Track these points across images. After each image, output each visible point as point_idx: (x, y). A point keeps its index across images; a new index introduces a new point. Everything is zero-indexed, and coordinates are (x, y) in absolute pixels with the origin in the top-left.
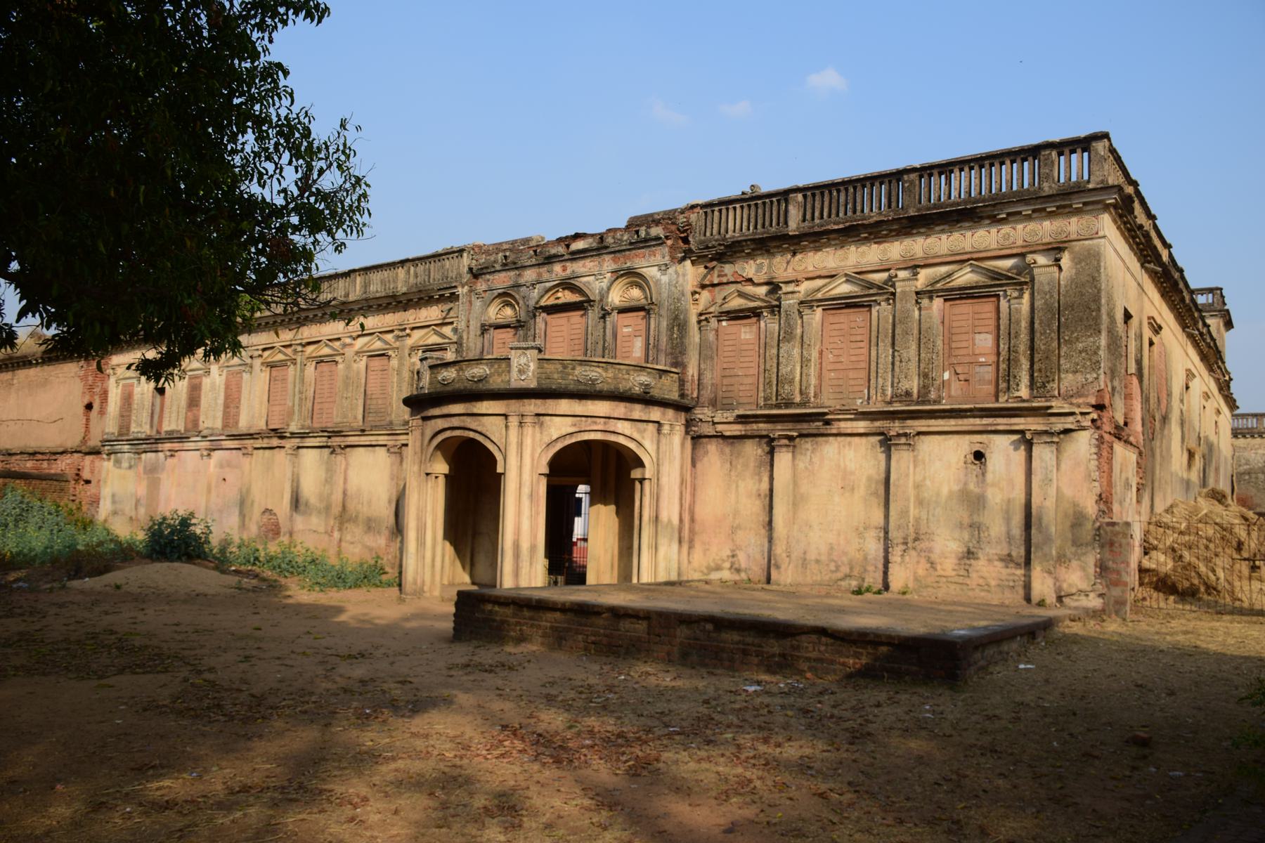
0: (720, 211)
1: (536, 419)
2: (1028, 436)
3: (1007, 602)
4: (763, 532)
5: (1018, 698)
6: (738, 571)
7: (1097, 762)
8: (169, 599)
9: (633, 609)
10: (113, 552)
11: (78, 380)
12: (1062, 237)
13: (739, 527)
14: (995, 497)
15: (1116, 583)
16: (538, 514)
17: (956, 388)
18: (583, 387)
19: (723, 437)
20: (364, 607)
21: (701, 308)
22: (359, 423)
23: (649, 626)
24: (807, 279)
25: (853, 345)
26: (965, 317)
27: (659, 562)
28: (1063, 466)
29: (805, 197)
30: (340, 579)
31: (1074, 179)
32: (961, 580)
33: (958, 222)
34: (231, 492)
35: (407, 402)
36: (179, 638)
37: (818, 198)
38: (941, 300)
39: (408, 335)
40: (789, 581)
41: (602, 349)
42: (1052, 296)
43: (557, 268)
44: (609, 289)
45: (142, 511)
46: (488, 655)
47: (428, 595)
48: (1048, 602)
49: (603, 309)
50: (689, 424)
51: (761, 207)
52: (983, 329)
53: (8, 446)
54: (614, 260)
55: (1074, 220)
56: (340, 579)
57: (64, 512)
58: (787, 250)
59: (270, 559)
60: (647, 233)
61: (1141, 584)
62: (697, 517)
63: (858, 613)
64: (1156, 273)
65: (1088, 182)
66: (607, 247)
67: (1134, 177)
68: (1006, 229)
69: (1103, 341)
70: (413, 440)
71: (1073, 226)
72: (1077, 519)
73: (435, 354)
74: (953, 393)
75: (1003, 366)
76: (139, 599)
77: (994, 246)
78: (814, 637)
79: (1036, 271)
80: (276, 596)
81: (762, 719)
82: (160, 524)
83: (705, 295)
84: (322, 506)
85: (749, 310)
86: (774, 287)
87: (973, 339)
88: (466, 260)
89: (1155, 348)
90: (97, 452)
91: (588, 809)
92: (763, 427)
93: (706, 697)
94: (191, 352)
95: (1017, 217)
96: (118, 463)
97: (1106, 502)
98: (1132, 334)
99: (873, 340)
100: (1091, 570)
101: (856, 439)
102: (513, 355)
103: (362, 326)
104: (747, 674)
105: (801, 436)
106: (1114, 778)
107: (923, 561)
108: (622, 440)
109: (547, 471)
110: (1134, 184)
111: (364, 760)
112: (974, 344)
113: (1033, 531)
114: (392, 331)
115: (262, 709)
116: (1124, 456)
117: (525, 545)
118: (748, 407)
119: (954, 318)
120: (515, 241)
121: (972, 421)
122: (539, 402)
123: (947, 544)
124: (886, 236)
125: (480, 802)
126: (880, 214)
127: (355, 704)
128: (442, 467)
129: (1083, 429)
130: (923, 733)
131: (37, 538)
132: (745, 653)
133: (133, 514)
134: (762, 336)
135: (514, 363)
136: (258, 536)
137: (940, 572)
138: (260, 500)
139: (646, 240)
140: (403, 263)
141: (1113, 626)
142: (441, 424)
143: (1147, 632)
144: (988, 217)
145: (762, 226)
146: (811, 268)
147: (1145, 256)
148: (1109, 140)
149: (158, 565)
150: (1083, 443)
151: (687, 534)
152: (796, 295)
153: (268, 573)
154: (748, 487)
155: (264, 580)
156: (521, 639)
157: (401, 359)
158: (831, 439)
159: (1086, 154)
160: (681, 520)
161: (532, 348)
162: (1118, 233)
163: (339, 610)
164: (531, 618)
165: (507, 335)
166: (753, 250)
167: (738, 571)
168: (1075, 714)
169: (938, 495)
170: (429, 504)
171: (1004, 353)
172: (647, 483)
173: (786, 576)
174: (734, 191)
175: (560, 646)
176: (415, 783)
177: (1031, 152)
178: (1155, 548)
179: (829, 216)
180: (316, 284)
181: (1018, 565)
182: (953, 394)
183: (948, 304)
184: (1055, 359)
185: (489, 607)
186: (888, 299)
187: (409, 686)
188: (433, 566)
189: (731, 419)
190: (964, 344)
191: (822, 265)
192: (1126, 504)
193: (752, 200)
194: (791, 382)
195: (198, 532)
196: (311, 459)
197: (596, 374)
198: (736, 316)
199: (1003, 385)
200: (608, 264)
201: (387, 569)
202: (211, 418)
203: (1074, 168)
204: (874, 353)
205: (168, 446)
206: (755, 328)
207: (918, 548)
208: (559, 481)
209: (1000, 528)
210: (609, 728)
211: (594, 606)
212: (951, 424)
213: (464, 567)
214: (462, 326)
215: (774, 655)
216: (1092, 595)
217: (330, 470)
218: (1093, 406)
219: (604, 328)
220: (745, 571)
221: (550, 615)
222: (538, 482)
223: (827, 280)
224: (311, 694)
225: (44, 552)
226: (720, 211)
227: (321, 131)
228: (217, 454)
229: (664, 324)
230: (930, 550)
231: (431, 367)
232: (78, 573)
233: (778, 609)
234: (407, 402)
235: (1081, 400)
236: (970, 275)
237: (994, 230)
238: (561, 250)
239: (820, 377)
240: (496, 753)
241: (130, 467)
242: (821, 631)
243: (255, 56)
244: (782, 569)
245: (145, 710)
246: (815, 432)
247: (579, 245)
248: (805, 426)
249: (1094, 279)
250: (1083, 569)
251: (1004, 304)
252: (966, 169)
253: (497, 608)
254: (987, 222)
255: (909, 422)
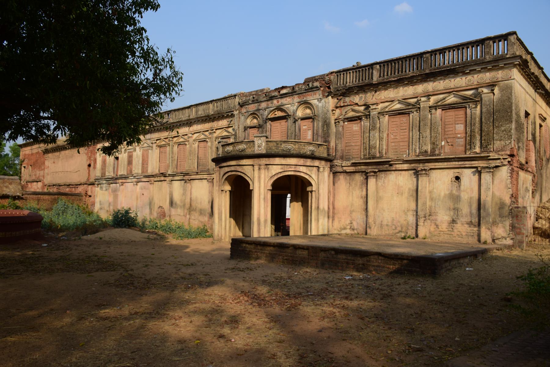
0: (344, 74)
1: (266, 167)
2: (479, 169)
3: (470, 242)
4: (364, 213)
5: (461, 282)
6: (353, 230)
7: (485, 308)
8: (120, 243)
9: (302, 245)
10: (100, 224)
11: (85, 155)
12: (495, 80)
13: (353, 211)
14: (465, 196)
15: (519, 234)
16: (267, 206)
17: (447, 149)
18: (285, 152)
19: (346, 172)
20: (197, 245)
21: (336, 117)
22: (196, 170)
23: (309, 253)
24: (382, 103)
25: (402, 131)
26: (451, 117)
27: (319, 226)
28: (495, 182)
29: (380, 66)
30: (189, 235)
31: (500, 53)
32: (449, 233)
33: (448, 75)
34: (146, 200)
35: (213, 160)
36: (122, 258)
37: (386, 67)
38: (441, 110)
39: (215, 132)
40: (375, 234)
41: (296, 136)
42: (490, 107)
43: (275, 101)
44: (297, 110)
45: (111, 208)
46: (243, 265)
47: (223, 241)
48: (488, 242)
49: (294, 119)
50: (331, 167)
51: (361, 71)
52: (459, 122)
53: (59, 182)
54: (299, 97)
55: (500, 72)
56: (189, 235)
57: (81, 209)
58: (373, 90)
59: (162, 227)
60: (313, 85)
61: (534, 234)
62: (336, 206)
63: (398, 246)
64: (543, 94)
65: (507, 54)
66: (295, 92)
67: (530, 50)
68: (469, 77)
69: (513, 126)
70: (215, 176)
71: (500, 74)
72: (501, 206)
73: (224, 140)
74: (446, 151)
75: (468, 138)
76: (109, 243)
77: (464, 85)
78: (376, 257)
79: (483, 96)
80: (163, 241)
81: (348, 289)
82: (118, 213)
83: (338, 111)
84: (182, 204)
85: (357, 117)
86: (367, 106)
87: (455, 127)
88: (237, 100)
89: (543, 128)
90: (93, 184)
91: (266, 322)
92: (363, 168)
93: (328, 281)
94: (120, 143)
95: (474, 72)
96: (101, 188)
97: (515, 198)
98: (530, 122)
99: (411, 129)
100: (508, 228)
101: (404, 172)
102: (255, 139)
103: (178, 132)
104: (347, 272)
105: (379, 171)
106: (488, 314)
107: (433, 224)
108: (302, 175)
109: (271, 188)
110: (531, 54)
111: (183, 303)
112: (455, 129)
113: (482, 211)
114: (208, 131)
115: (149, 285)
116: (525, 179)
117: (262, 220)
118: (357, 159)
119: (446, 118)
120: (258, 91)
121: (454, 163)
122: (267, 159)
123: (443, 217)
124: (416, 82)
125: (224, 319)
126: (413, 73)
127: (185, 283)
128: (228, 188)
129: (504, 165)
130: (414, 295)
131: (70, 219)
132: (348, 263)
133: (108, 209)
134: (362, 128)
135: (256, 143)
136: (157, 217)
137: (441, 230)
138: (157, 202)
139: (312, 88)
140: (211, 101)
141: (516, 252)
142: (227, 169)
143: (531, 255)
144: (461, 72)
145: (362, 80)
146: (383, 98)
147: (537, 87)
148: (517, 35)
149: (117, 230)
150: (504, 172)
151: (331, 214)
152: (377, 110)
153: (160, 232)
154: (357, 194)
155: (159, 235)
156: (257, 258)
157: (212, 142)
158: (393, 172)
159: (506, 42)
160: (329, 208)
161: (263, 136)
162: (522, 77)
163: (187, 247)
164: (261, 250)
165: (255, 131)
166: (358, 91)
167: (353, 230)
168: (483, 288)
169: (439, 196)
170: (223, 203)
171: (469, 133)
172: (313, 193)
173: (374, 232)
174: (350, 66)
175: (273, 261)
176: (202, 312)
177: (481, 42)
178: (541, 218)
179: (391, 74)
180: (161, 115)
181: (475, 226)
182: (446, 151)
183: (444, 111)
184: (491, 134)
185: (244, 245)
186: (417, 110)
187: (208, 276)
188: (225, 229)
189: (349, 165)
190: (451, 129)
191: (388, 96)
192: (526, 199)
193: (357, 69)
194: (375, 148)
195: (132, 216)
196: (177, 185)
197: (291, 147)
198: (351, 120)
199: (468, 147)
200: (296, 99)
201: (209, 230)
202: (137, 169)
203: (501, 48)
204: (411, 134)
205: (120, 181)
206: (359, 125)
207: (431, 219)
208: (277, 192)
209: (467, 209)
210: (284, 293)
211: (286, 244)
212: (445, 165)
213: (239, 229)
214: (236, 127)
215: (359, 264)
216: (508, 239)
217: (185, 190)
218: (509, 155)
219: (295, 127)
220: (356, 229)
221: (268, 248)
222: (267, 193)
223: (390, 103)
224: (169, 279)
225: (74, 225)
226: (344, 74)
227: (161, 53)
228: (140, 184)
229: (320, 124)
230: (436, 220)
231: (222, 146)
232: (86, 234)
233: (364, 245)
234: (213, 160)
235: (503, 153)
236: (453, 98)
237: (464, 78)
238: (276, 94)
239: (388, 145)
240: (235, 301)
241: (106, 190)
242: (379, 254)
243: (135, 24)
244: (372, 229)
245: (104, 285)
246: (385, 169)
247: (284, 91)
248: (381, 167)
249: (509, 98)
250: (504, 227)
251: (468, 110)
252: (452, 51)
253: (247, 245)
254: (461, 74)
255: (427, 164)
